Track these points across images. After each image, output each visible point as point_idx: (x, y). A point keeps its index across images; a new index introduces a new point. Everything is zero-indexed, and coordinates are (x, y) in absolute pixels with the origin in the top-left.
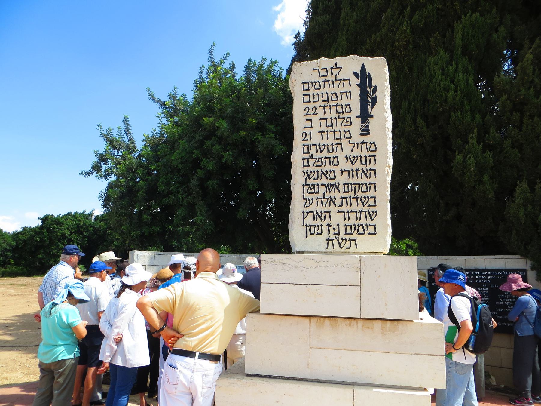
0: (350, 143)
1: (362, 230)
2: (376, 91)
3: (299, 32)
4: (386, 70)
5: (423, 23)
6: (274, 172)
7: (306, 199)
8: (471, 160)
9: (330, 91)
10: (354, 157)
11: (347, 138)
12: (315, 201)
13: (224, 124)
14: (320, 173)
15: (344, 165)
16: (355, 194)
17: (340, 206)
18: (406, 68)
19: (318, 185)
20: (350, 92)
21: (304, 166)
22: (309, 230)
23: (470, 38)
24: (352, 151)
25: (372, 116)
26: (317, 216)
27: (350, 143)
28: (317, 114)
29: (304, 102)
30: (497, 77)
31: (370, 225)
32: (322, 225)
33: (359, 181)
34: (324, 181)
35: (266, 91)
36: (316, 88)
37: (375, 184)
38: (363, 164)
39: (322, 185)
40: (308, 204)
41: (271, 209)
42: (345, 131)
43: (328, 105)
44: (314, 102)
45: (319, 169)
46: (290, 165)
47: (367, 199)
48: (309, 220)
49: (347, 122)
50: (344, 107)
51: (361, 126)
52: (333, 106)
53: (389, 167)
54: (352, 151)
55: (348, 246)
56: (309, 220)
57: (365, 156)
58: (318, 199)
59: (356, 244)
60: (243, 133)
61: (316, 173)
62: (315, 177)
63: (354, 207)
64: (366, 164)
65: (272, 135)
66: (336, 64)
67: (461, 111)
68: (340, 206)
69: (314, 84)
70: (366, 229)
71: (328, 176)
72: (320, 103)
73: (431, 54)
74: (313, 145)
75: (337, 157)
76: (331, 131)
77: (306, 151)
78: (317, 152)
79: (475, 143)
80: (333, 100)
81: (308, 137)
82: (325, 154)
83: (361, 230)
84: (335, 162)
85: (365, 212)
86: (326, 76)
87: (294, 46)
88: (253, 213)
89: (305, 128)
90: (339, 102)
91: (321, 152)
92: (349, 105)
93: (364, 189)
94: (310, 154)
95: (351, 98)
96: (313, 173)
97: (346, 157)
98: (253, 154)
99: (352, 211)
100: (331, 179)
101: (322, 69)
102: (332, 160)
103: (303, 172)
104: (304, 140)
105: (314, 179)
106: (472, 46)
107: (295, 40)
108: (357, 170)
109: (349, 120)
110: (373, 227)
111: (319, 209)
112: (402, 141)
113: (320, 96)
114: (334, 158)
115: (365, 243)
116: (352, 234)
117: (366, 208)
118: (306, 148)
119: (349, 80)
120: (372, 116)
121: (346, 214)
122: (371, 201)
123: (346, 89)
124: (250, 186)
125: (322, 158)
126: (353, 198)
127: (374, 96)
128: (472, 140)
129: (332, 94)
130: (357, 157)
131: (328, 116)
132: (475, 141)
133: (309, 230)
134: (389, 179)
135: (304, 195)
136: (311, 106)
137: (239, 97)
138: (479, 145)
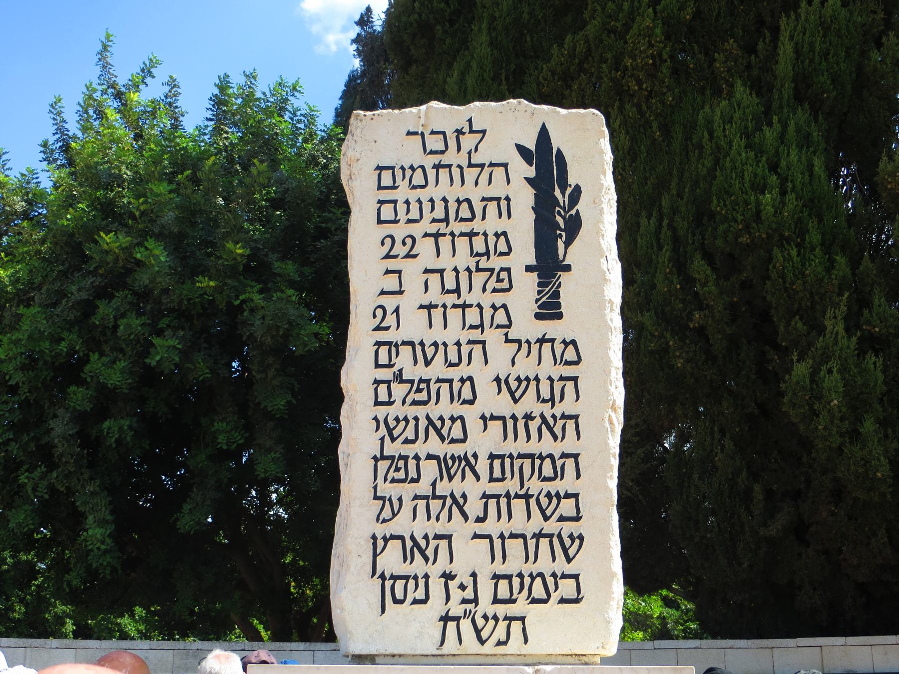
0: (507, 341)
1: (544, 589)
2: (579, 198)
3: (369, 10)
4: (605, 144)
5: (690, 10)
6: (289, 398)
7: (382, 498)
8: (832, 381)
9: (455, 192)
10: (518, 379)
11: (498, 326)
12: (408, 505)
13: (157, 254)
14: (423, 423)
15: (493, 401)
16: (522, 486)
17: (479, 520)
18: (655, 124)
19: (417, 458)
20: (508, 199)
21: (377, 403)
22: (392, 590)
23: (817, 57)
24: (513, 363)
25: (568, 268)
26: (414, 548)
27: (507, 341)
28: (415, 256)
29: (380, 222)
30: (885, 158)
31: (564, 576)
32: (426, 577)
33: (533, 447)
34: (434, 445)
35: (274, 164)
36: (414, 182)
37: (576, 456)
38: (544, 401)
39: (429, 457)
40: (387, 513)
41: (280, 502)
42: (493, 306)
43: (448, 231)
44: (409, 221)
45: (420, 412)
46: (339, 398)
47: (555, 500)
48: (392, 560)
49: (499, 280)
50: (492, 240)
51: (539, 292)
52: (462, 234)
53: (614, 408)
54: (513, 363)
55: (503, 638)
56: (392, 560)
57: (550, 379)
58: (416, 497)
59: (524, 630)
60: (207, 283)
61: (412, 423)
62: (410, 434)
63: (519, 523)
64: (552, 399)
65: (291, 292)
66: (470, 121)
67: (798, 245)
68: (479, 520)
69: (408, 173)
70: (551, 587)
71: (444, 432)
72: (426, 226)
73: (717, 93)
74: (404, 343)
75: (470, 379)
76: (455, 306)
77: (383, 359)
78: (416, 362)
79: (842, 332)
80: (462, 220)
81: (391, 320)
82: (438, 369)
83: (538, 590)
84: (467, 394)
85: (551, 536)
86: (442, 152)
87: (354, 46)
88: (229, 510)
89: (383, 293)
90: (477, 225)
91: (427, 363)
92: (505, 234)
93: (548, 470)
94: (395, 369)
95: (509, 216)
96: (403, 423)
97: (497, 380)
98: (231, 344)
99: (513, 536)
100: (453, 441)
101: (433, 133)
102: (456, 385)
103: (376, 419)
104: (378, 328)
105: (407, 441)
106: (822, 79)
107: (358, 29)
108: (528, 417)
109: (504, 275)
110: (573, 581)
111: (421, 527)
112: (647, 319)
113: (427, 207)
114: (462, 381)
115: (551, 629)
116: (514, 601)
117: (551, 527)
118: (383, 350)
119: (505, 165)
120: (568, 268)
121: (497, 543)
122: (567, 507)
123: (498, 189)
124: (222, 438)
125: (428, 382)
126: (517, 496)
127: (573, 212)
128: (834, 324)
129: (459, 202)
130: (527, 379)
131: (446, 261)
132: (840, 327)
133: (392, 590)
134: (614, 442)
135: (375, 488)
136: (400, 231)
137: (195, 180)
138: (849, 338)
